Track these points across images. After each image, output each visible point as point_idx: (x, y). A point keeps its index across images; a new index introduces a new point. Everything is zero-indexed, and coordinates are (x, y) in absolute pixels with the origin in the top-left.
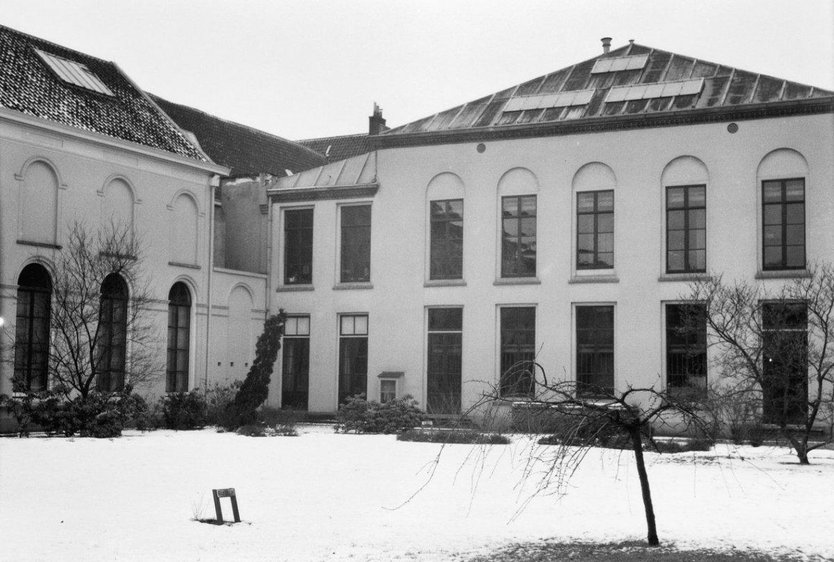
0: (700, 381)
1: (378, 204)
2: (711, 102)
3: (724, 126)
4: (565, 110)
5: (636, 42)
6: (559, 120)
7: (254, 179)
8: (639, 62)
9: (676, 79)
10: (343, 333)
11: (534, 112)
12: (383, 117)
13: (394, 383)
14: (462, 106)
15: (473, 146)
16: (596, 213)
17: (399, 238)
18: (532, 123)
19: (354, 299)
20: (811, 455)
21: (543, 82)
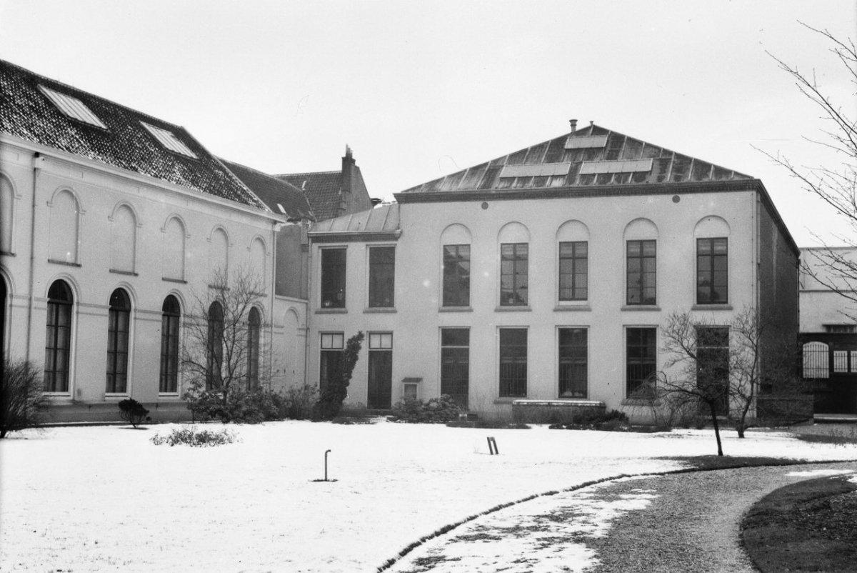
0: (653, 385)
1: (401, 248)
2: (660, 179)
3: (670, 197)
4: (549, 178)
5: (595, 123)
6: (545, 187)
7: (295, 223)
8: (601, 141)
9: (631, 158)
10: (371, 347)
11: (525, 179)
12: (354, 157)
13: (415, 386)
14: (465, 170)
15: (478, 204)
16: (574, 258)
17: (419, 277)
18: (525, 188)
19: (381, 321)
20: (746, 433)
21: (527, 153)
